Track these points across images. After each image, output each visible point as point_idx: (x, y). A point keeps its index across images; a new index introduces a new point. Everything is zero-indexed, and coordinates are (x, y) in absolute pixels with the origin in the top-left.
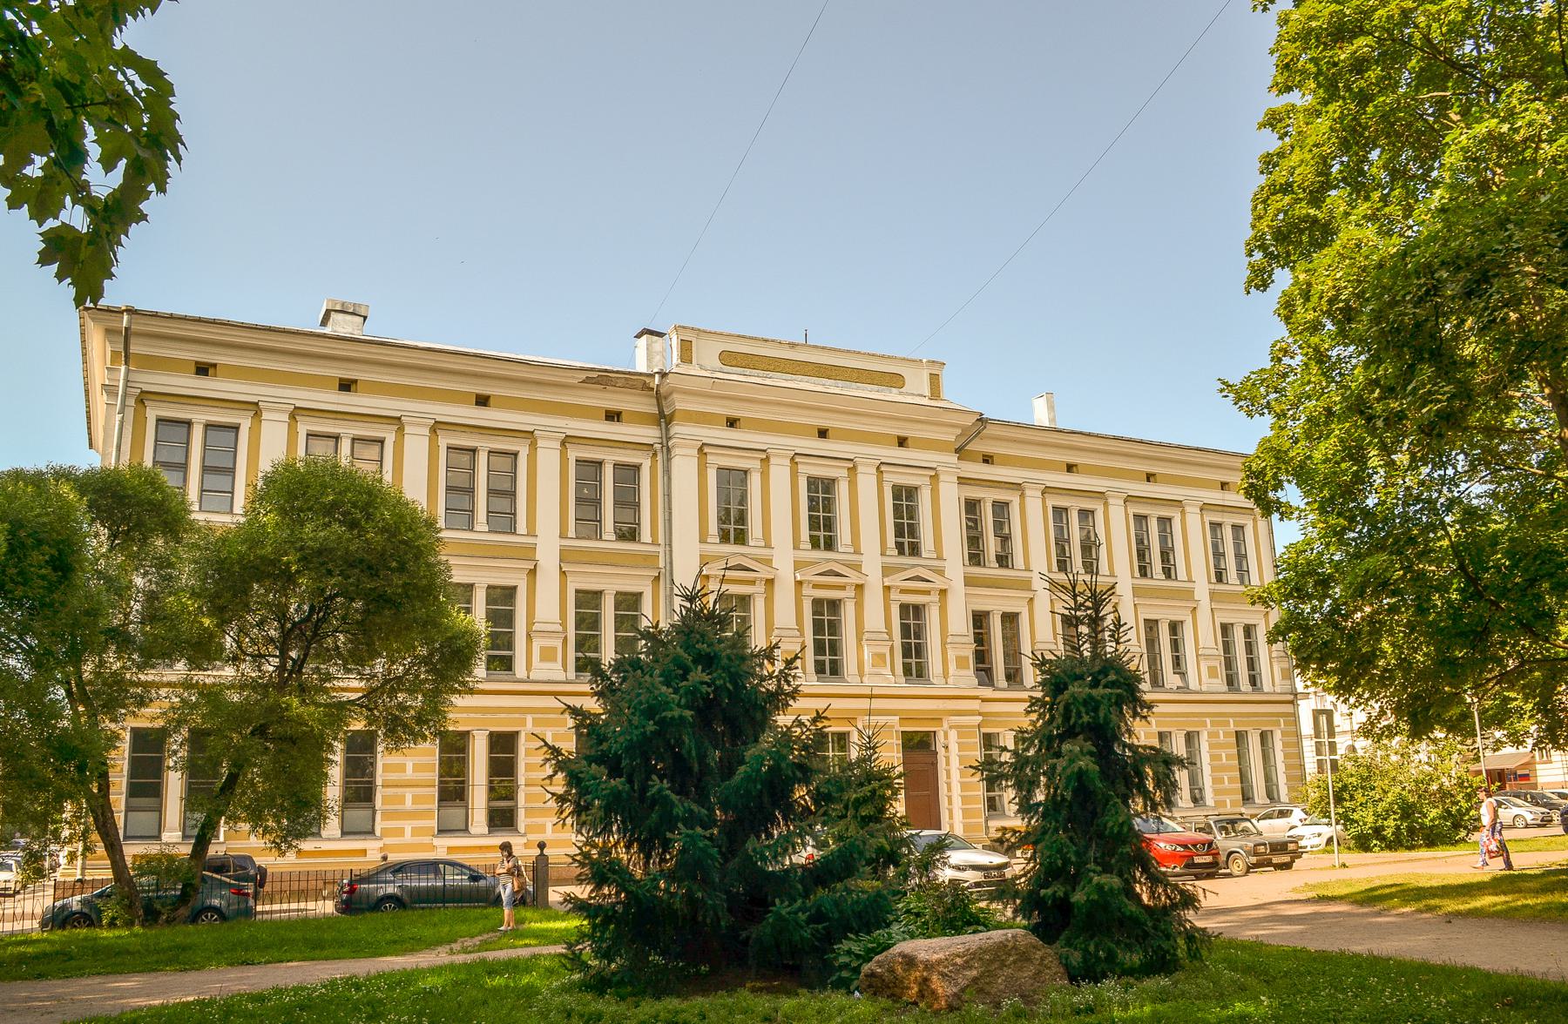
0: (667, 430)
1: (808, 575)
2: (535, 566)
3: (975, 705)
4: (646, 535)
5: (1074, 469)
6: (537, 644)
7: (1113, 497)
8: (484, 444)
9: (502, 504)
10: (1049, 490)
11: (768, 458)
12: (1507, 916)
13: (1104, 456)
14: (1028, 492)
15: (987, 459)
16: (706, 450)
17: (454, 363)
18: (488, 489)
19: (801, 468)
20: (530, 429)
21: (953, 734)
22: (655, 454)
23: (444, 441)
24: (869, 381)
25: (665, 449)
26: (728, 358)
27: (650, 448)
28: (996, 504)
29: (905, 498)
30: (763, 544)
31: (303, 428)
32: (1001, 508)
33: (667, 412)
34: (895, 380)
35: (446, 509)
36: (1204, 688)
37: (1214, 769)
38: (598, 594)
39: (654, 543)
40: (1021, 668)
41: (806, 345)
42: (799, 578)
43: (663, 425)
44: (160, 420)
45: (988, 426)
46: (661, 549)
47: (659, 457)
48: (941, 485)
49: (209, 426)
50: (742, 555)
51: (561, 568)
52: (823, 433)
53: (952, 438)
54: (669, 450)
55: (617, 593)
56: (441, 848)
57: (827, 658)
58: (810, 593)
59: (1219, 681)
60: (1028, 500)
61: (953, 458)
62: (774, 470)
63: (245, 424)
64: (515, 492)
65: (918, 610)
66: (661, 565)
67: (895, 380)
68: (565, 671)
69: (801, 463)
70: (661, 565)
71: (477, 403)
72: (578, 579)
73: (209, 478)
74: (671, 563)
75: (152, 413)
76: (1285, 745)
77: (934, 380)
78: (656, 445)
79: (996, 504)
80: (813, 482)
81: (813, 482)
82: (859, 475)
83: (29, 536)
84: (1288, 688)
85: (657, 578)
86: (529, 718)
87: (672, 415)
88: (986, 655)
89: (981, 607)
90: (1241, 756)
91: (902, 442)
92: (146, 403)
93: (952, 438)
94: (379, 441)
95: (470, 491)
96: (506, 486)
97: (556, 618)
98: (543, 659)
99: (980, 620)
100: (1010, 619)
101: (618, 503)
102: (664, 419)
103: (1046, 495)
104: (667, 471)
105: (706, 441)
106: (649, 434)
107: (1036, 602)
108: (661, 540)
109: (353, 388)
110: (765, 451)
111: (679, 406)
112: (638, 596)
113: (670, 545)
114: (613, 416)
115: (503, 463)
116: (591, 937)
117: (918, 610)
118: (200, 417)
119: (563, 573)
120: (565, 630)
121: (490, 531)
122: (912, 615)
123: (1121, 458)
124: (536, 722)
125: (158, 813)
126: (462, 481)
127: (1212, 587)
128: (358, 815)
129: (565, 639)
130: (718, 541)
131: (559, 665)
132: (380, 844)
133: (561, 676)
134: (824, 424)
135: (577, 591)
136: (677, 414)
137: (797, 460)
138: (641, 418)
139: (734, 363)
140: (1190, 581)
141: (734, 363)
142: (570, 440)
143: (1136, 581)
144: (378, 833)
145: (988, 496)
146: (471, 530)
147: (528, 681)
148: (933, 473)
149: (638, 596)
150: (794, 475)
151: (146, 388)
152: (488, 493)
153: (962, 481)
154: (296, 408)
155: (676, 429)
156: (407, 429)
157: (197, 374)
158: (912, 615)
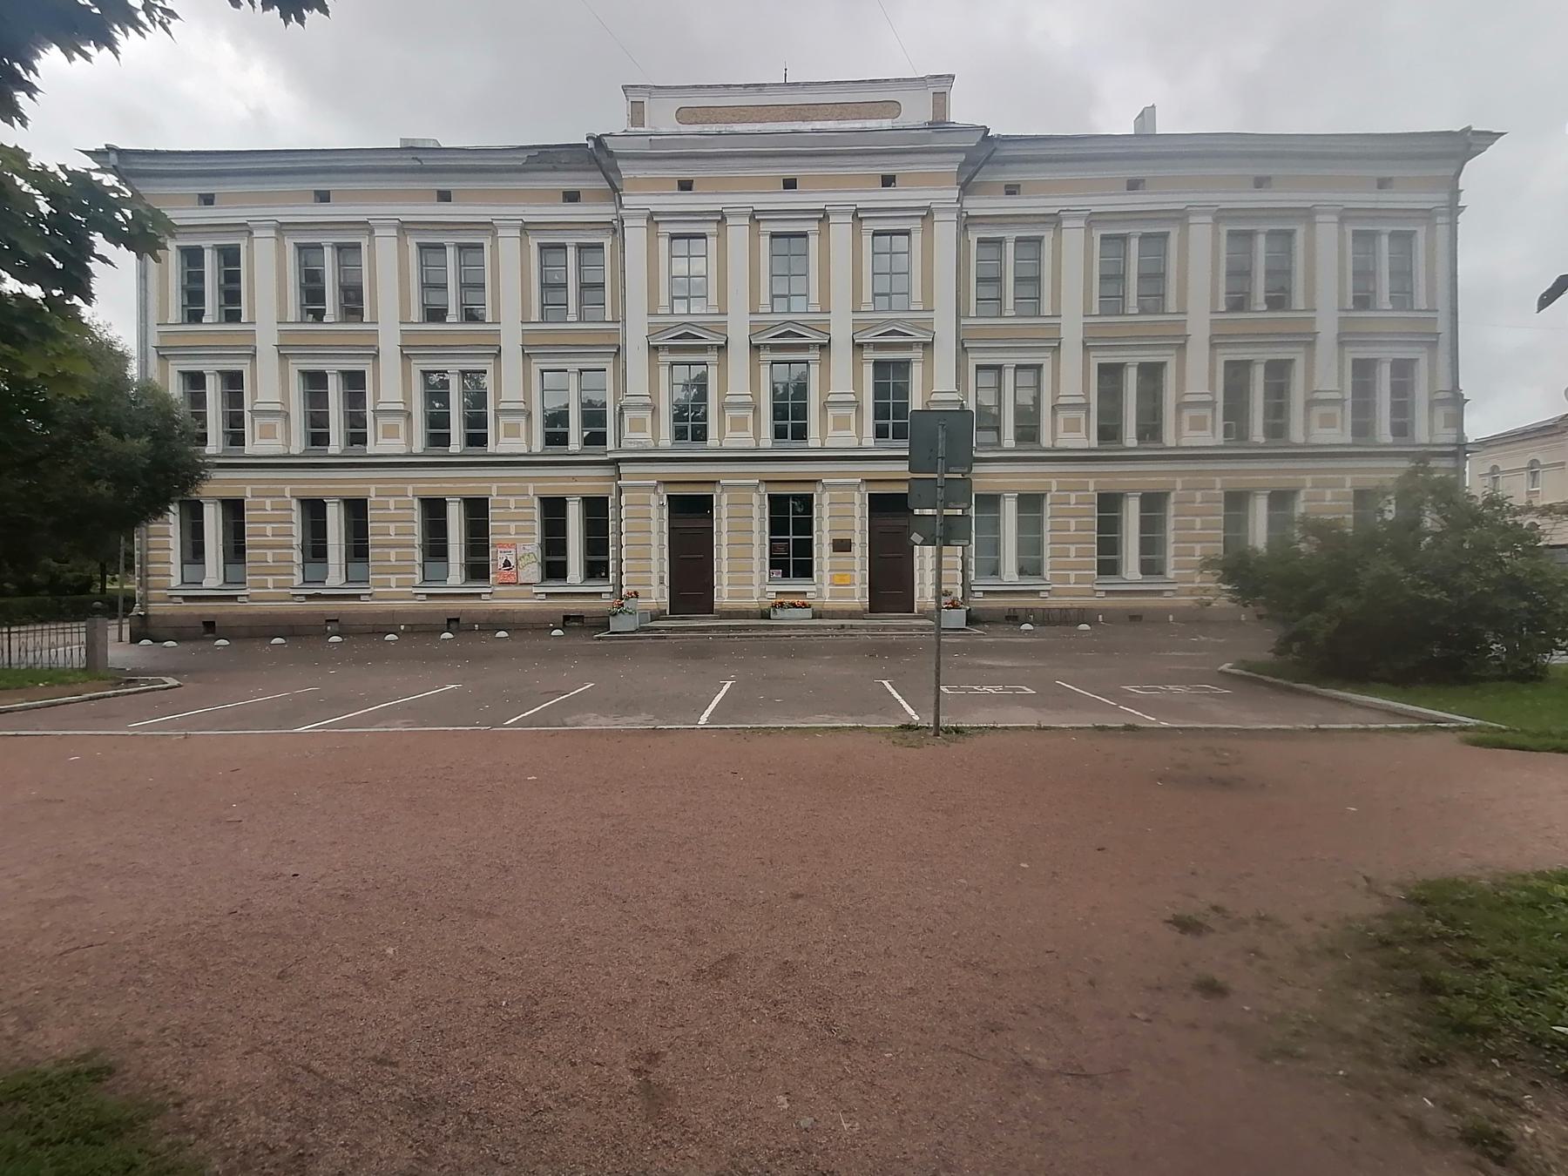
1: (867, 338)
2: (1060, 343)
5: (1141, 185)
9: (1028, 291)
10: (285, 227)
12: (1420, 730)
15: (1012, 190)
26: (684, 115)
34: (891, 108)
35: (977, 299)
38: (1247, 365)
44: (980, 241)
49: (1018, 240)
53: (955, 168)
67: (891, 108)
68: (1088, 439)
71: (1008, 193)
72: (1228, 351)
75: (973, 237)
78: (614, 222)
88: (428, 425)
95: (998, 280)
114: (572, 197)
116: (72, 668)
118: (1010, 235)
131: (1209, 432)
134: (790, 173)
135: (1100, 365)
138: (599, 197)
139: (935, 109)
152: (1015, 281)
157: (564, 201)
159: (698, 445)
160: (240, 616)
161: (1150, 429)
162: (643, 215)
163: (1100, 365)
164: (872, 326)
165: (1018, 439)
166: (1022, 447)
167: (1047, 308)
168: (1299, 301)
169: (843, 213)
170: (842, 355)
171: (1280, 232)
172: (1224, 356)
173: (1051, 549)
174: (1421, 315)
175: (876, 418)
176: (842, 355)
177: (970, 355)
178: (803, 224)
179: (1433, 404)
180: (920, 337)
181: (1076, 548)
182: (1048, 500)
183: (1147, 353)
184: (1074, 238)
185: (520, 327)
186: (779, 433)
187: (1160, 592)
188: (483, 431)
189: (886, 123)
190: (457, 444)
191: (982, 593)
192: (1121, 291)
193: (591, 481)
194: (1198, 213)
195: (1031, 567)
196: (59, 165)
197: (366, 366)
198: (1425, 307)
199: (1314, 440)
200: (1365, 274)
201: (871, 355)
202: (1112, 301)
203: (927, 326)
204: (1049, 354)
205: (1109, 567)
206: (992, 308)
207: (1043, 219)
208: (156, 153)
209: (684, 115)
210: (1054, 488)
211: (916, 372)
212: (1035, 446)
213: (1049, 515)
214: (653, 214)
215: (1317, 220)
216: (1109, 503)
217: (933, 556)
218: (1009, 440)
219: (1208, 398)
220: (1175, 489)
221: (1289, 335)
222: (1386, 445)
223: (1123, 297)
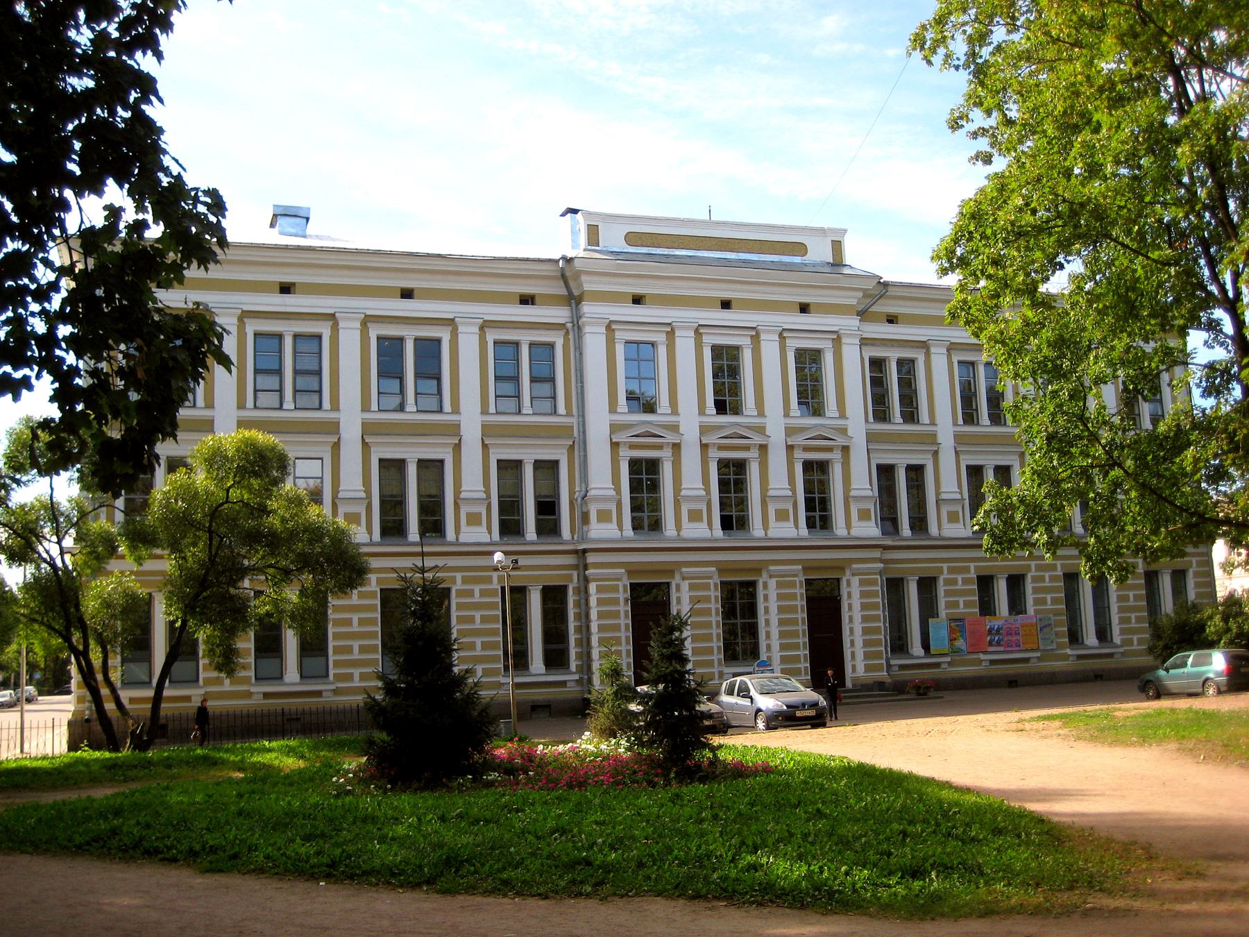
0: (577, 309)
1: (798, 440)
3: (876, 554)
8: (525, 337)
11: (673, 331)
13: (383, 274)
14: (933, 350)
15: (892, 320)
16: (614, 327)
17: (520, 269)
18: (255, 369)
19: (706, 339)
20: (332, 311)
21: (772, 583)
22: (567, 333)
23: (491, 337)
24: (681, 246)
25: (576, 327)
28: (900, 362)
29: (808, 362)
30: (837, 415)
31: (374, 333)
32: (907, 367)
33: (576, 293)
34: (801, 249)
36: (462, 539)
37: (1121, 609)
38: (518, 464)
39: (569, 414)
40: (926, 517)
42: (614, 440)
43: (574, 305)
44: (257, 335)
45: (890, 289)
47: (571, 336)
48: (678, 341)
51: (363, 439)
52: (726, 305)
54: (579, 328)
55: (536, 461)
57: (817, 514)
58: (800, 456)
59: (873, 523)
60: (933, 357)
61: (854, 322)
62: (679, 342)
63: (446, 337)
64: (518, 377)
65: (823, 466)
66: (576, 434)
70: (576, 434)
73: (300, 379)
74: (584, 432)
76: (1197, 585)
77: (837, 246)
79: (900, 362)
80: (717, 351)
81: (717, 351)
82: (677, 339)
83: (1149, 444)
85: (572, 448)
86: (459, 576)
87: (582, 294)
89: (887, 459)
91: (804, 308)
93: (854, 302)
95: (516, 379)
97: (358, 484)
98: (469, 523)
99: (885, 473)
100: (915, 472)
101: (418, 375)
102: (573, 300)
103: (952, 352)
104: (579, 349)
105: (613, 318)
106: (560, 314)
107: (941, 454)
109: (292, 289)
110: (670, 324)
111: (587, 287)
112: (554, 464)
113: (583, 416)
117: (823, 466)
119: (485, 446)
120: (489, 497)
121: (534, 414)
122: (816, 472)
123: (345, 272)
124: (465, 580)
125: (148, 664)
126: (308, 363)
127: (958, 429)
128: (314, 662)
129: (619, 505)
130: (714, 412)
132: (202, 691)
133: (705, 533)
134: (726, 295)
135: (381, 460)
136: (585, 295)
137: (613, 327)
138: (551, 300)
142: (487, 324)
143: (958, 429)
144: (331, 677)
145: (893, 356)
147: (457, 543)
149: (554, 464)
150: (610, 343)
153: (864, 342)
154: (366, 316)
155: (588, 308)
156: (341, 324)
158: (816, 472)
159: (654, 535)
160: (1113, 666)
161: (919, 522)
162: (775, 331)
163: (381, 460)
164: (802, 430)
165: (422, 533)
168: (924, 416)
169: (688, 328)
175: (807, 510)
176: (777, 459)
178: (823, 342)
180: (841, 441)
182: (941, 582)
183: (428, 450)
184: (939, 361)
186: (637, 526)
187: (1026, 660)
188: (634, 514)
189: (797, 260)
190: (906, 530)
194: (768, 332)
195: (1103, 633)
199: (771, 534)
203: (843, 431)
206: (511, 404)
208: (910, 286)
209: (631, 238)
210: (1194, 565)
212: (555, 540)
219: (958, 496)
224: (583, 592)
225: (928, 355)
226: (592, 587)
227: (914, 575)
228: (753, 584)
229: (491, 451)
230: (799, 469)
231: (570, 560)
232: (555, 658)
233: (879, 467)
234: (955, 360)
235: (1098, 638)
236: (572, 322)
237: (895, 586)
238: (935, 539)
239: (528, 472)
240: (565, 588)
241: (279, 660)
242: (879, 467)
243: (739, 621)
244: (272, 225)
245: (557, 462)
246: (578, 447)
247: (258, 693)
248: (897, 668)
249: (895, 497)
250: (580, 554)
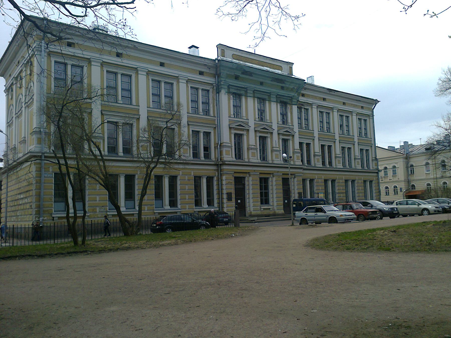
1: (258, 129)
2: (91, 111)
4: (211, 113)
6: (141, 144)
7: (182, 79)
20: (136, 67)
27: (176, 78)
35: (122, 97)
38: (198, 132)
41: (255, 54)
43: (217, 78)
46: (216, 118)
50: (241, 121)
56: (197, 209)
63: (310, 108)
67: (280, 68)
69: (231, 88)
71: (200, 74)
84: (375, 167)
85: (215, 128)
90: (365, 187)
92: (51, 55)
94: (81, 67)
95: (197, 102)
96: (63, 77)
108: (216, 116)
109: (72, 45)
115: (126, 79)
126: (126, 87)
134: (262, 80)
137: (230, 87)
140: (335, 133)
141: (236, 58)
146: (116, 103)
148: (290, 98)
151: (104, 60)
154: (103, 62)
166: (110, 155)
167: (134, 102)
170: (252, 133)
171: (206, 90)
172: (259, 134)
173: (88, 197)
174: (331, 134)
176: (252, 133)
177: (105, 117)
179: (372, 160)
181: (302, 193)
182: (179, 178)
185: (228, 118)
188: (205, 152)
191: (111, 216)
192: (208, 107)
193: (210, 170)
196: (379, 101)
197: (352, 147)
198: (152, 107)
200: (195, 101)
201: (234, 131)
202: (196, 110)
204: (135, 120)
205: (198, 203)
207: (198, 82)
211: (245, 137)
213: (137, 183)
214: (278, 95)
215: (92, 64)
216: (197, 179)
217: (138, 200)
218: (121, 153)
220: (180, 175)
221: (343, 141)
222: (120, 157)
223: (197, 108)
224: (220, 180)
225: (312, 108)
226: (224, 178)
227: (123, 174)
228: (244, 178)
229: (190, 127)
230: (258, 138)
231: (215, 168)
232: (210, 203)
233: (321, 145)
234: (318, 110)
235: (207, 204)
236: (216, 84)
237: (304, 180)
238: (292, 165)
239: (201, 135)
240: (134, 176)
241: (161, 201)
242: (321, 145)
243: (264, 191)
244: (190, 48)
245: (210, 133)
246: (217, 127)
247: (157, 213)
248: (57, 218)
249: (310, 152)
250: (219, 166)
